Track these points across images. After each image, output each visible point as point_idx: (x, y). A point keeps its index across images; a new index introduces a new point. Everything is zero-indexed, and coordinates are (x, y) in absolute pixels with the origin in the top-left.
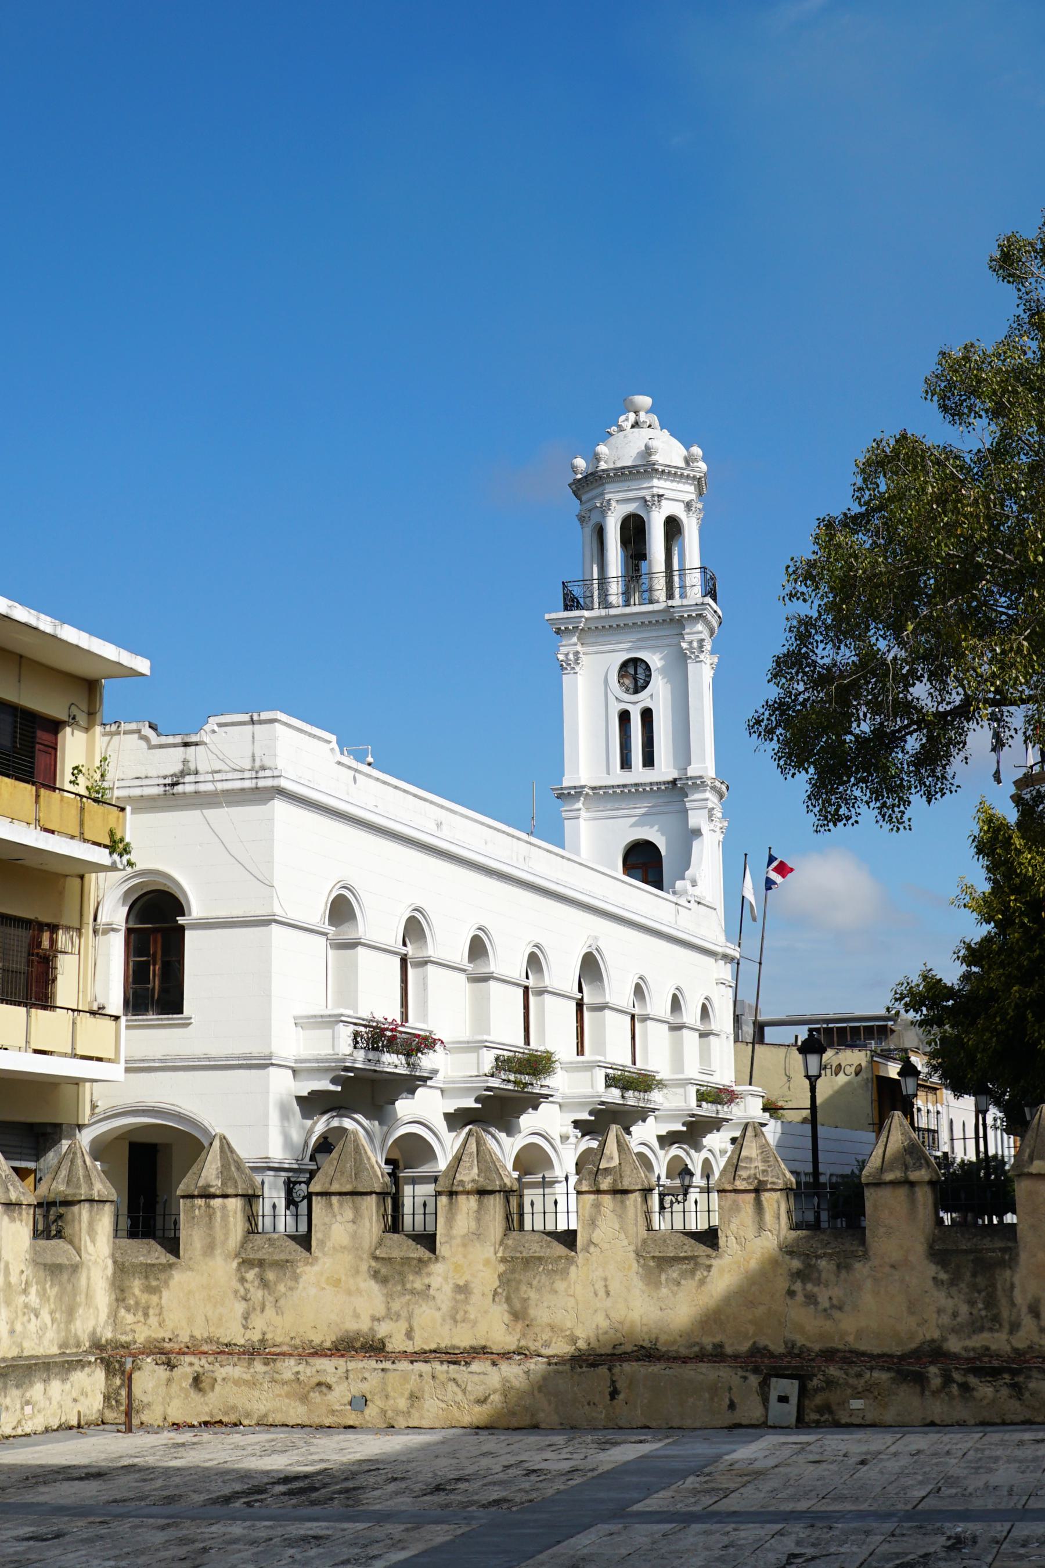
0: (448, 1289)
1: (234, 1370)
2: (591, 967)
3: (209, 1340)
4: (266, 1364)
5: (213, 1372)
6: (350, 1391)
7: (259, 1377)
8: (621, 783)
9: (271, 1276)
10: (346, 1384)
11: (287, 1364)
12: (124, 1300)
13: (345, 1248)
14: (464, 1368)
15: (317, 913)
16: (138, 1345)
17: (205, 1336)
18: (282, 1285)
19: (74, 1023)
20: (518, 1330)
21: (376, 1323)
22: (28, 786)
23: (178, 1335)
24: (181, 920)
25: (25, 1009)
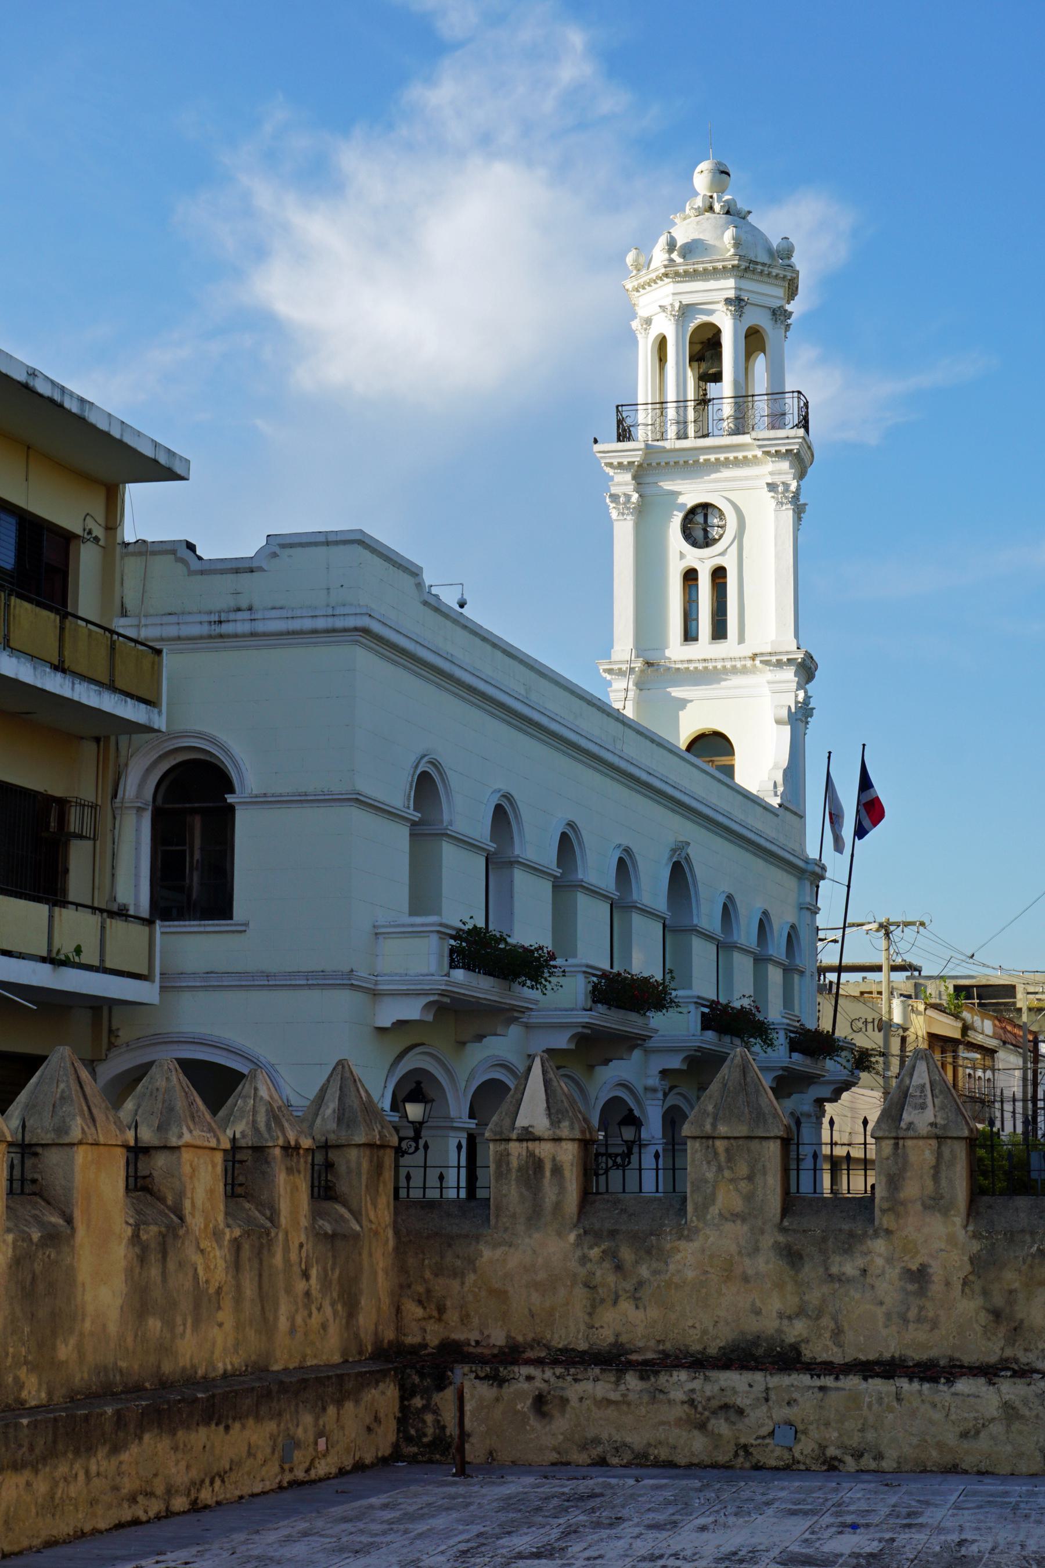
0: (894, 1273)
1: (596, 1386)
2: (680, 874)
3: (537, 1342)
4: (642, 1378)
5: (563, 1389)
6: (771, 1418)
7: (632, 1397)
8: (701, 658)
9: (627, 1254)
10: (764, 1408)
11: (675, 1378)
12: (409, 1286)
13: (737, 1215)
14: (945, 1388)
15: (397, 793)
16: (430, 1350)
17: (530, 1336)
18: (644, 1267)
19: (103, 928)
20: (1001, 1335)
21: (786, 1322)
22: (52, 615)
23: (489, 1336)
24: (230, 799)
25: (47, 907)
